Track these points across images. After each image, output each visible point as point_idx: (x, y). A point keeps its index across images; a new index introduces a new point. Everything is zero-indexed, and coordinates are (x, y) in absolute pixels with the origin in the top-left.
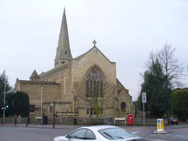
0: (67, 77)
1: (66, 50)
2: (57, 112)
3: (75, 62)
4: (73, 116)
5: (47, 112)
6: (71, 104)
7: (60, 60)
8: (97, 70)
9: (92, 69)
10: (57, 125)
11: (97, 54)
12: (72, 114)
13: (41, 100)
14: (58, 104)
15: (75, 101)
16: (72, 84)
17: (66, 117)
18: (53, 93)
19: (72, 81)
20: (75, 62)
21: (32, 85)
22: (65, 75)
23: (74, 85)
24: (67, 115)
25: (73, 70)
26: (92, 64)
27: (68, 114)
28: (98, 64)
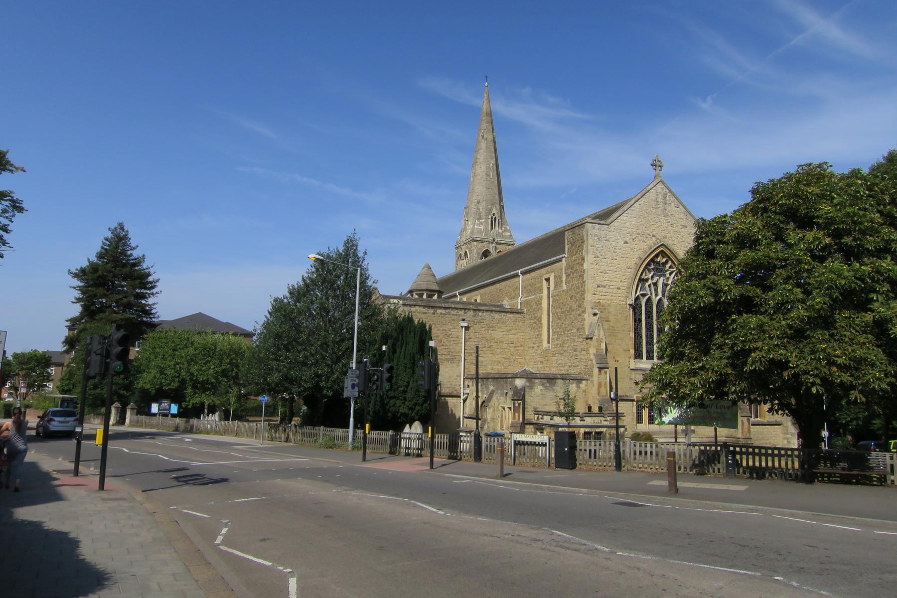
0: (557, 285)
1: (494, 214)
2: (537, 413)
3: (595, 232)
4: (604, 430)
5: (492, 410)
6: (584, 382)
7: (475, 243)
8: (667, 262)
9: (652, 260)
10: (70, 469)
11: (668, 208)
12: (602, 419)
13: (458, 366)
14: (559, 381)
15: (600, 369)
16: (589, 311)
17: (582, 430)
18: (502, 342)
19: (589, 297)
20: (595, 232)
21: (431, 311)
22: (548, 280)
23: (595, 314)
24: (582, 422)
25: (589, 258)
26: (651, 242)
27: (589, 421)
28: (671, 243)
